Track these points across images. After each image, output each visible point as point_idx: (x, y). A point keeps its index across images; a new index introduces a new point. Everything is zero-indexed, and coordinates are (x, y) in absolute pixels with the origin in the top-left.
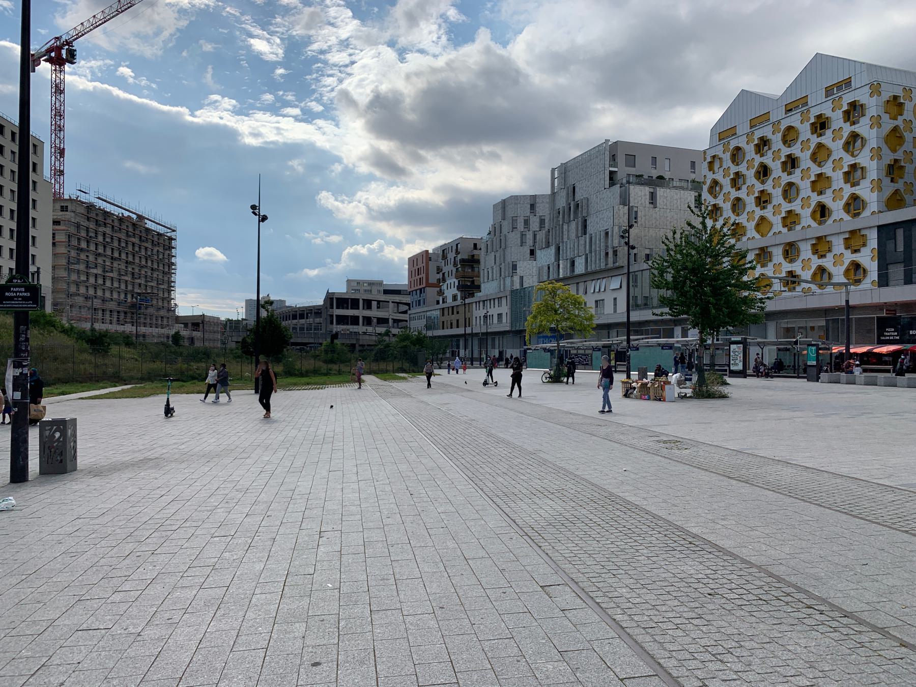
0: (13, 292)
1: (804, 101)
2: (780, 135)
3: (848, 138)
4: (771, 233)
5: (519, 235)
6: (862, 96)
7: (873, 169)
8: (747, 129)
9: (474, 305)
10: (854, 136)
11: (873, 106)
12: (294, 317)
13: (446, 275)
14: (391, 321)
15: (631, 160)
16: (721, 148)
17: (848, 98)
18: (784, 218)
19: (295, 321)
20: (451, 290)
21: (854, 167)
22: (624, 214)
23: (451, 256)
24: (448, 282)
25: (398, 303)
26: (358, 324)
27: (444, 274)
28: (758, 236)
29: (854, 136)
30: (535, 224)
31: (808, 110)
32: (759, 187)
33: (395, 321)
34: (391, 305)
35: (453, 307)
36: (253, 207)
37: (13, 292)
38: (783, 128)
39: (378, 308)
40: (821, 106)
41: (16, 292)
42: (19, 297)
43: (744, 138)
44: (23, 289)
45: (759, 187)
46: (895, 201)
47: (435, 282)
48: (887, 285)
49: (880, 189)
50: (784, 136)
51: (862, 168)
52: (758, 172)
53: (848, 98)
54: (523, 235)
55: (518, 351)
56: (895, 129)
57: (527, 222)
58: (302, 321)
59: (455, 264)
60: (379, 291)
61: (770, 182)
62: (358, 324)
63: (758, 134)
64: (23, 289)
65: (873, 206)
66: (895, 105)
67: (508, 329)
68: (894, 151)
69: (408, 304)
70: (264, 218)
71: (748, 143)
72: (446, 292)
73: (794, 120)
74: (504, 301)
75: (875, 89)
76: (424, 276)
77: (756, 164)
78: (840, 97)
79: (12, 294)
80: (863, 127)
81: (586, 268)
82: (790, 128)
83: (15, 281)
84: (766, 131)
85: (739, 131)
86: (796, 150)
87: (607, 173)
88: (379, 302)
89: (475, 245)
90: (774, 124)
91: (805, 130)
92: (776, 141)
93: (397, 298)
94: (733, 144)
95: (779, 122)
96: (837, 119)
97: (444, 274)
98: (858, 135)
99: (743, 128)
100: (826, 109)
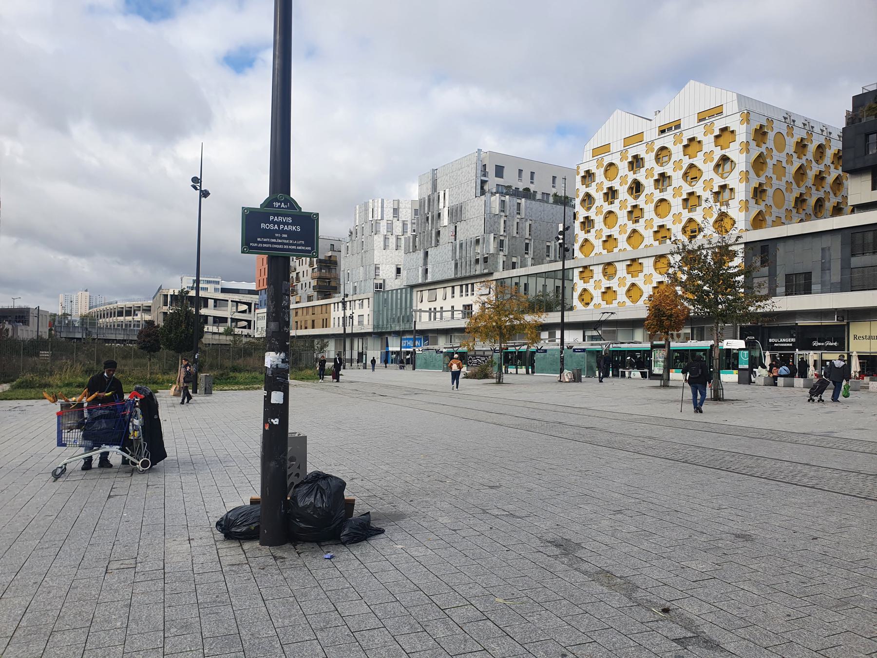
0: (274, 223)
1: (677, 123)
2: (653, 155)
3: (718, 161)
4: (642, 246)
5: (382, 239)
6: (734, 122)
7: (741, 191)
8: (621, 147)
10: (725, 159)
11: (742, 133)
12: (120, 314)
13: (301, 275)
14: (229, 320)
15: (499, 171)
16: (594, 163)
17: (719, 123)
18: (655, 232)
19: (121, 318)
21: (723, 187)
25: (237, 302)
27: (297, 274)
28: (629, 248)
29: (725, 159)
30: (398, 228)
31: (681, 133)
32: (631, 202)
33: (233, 320)
34: (230, 303)
36: (195, 180)
37: (274, 223)
38: (656, 148)
39: (215, 306)
40: (692, 128)
41: (279, 224)
42: (283, 232)
43: (618, 155)
44: (290, 220)
45: (631, 202)
46: (758, 222)
48: (811, 293)
49: (747, 209)
50: (657, 155)
51: (732, 189)
52: (631, 188)
53: (719, 124)
54: (386, 238)
55: (379, 352)
56: (760, 156)
57: (390, 227)
58: (129, 318)
60: (216, 290)
61: (642, 197)
63: (632, 152)
64: (290, 220)
65: (741, 224)
66: (760, 134)
67: (371, 330)
68: (758, 176)
69: (249, 304)
70: (205, 194)
71: (621, 160)
72: (300, 291)
73: (667, 140)
74: (366, 302)
75: (747, 118)
77: (630, 181)
78: (712, 123)
79: (271, 227)
80: (733, 151)
81: (456, 273)
82: (663, 148)
83: (277, 204)
84: (639, 150)
85: (613, 149)
86: (668, 169)
87: (479, 182)
88: (216, 300)
90: (647, 143)
91: (677, 151)
92: (649, 160)
93: (237, 297)
94: (607, 160)
95: (652, 142)
96: (708, 143)
97: (297, 274)
98: (728, 159)
99: (617, 146)
100: (698, 133)
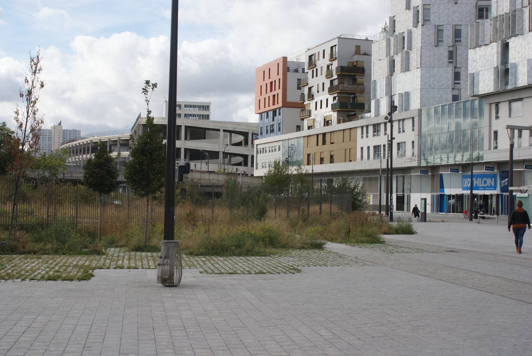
9: (359, 131)
13: (314, 90)
20: (322, 109)
22: (518, 20)
23: (322, 63)
24: (317, 99)
26: (186, 150)
35: (324, 135)
44: (400, 194)
47: (298, 100)
48: (205, 139)
58: (47, 139)
59: (329, 74)
62: (186, 150)
67: (415, 164)
72: (313, 112)
76: (280, 92)
89: (358, 48)
97: (310, 89)
